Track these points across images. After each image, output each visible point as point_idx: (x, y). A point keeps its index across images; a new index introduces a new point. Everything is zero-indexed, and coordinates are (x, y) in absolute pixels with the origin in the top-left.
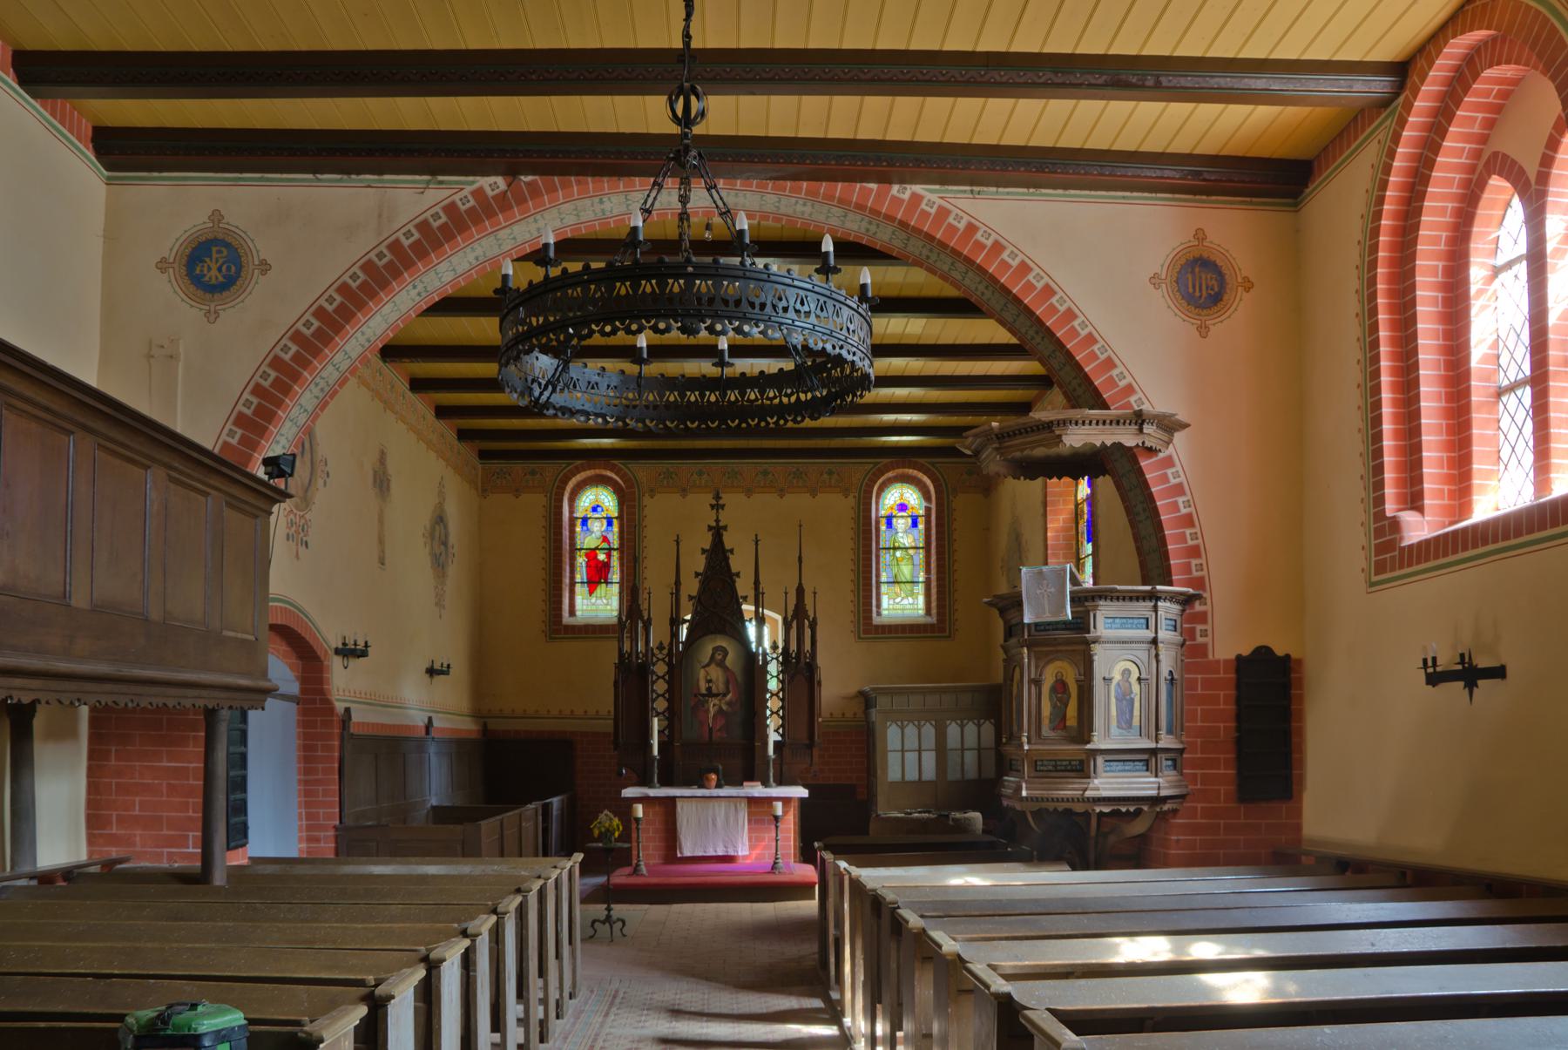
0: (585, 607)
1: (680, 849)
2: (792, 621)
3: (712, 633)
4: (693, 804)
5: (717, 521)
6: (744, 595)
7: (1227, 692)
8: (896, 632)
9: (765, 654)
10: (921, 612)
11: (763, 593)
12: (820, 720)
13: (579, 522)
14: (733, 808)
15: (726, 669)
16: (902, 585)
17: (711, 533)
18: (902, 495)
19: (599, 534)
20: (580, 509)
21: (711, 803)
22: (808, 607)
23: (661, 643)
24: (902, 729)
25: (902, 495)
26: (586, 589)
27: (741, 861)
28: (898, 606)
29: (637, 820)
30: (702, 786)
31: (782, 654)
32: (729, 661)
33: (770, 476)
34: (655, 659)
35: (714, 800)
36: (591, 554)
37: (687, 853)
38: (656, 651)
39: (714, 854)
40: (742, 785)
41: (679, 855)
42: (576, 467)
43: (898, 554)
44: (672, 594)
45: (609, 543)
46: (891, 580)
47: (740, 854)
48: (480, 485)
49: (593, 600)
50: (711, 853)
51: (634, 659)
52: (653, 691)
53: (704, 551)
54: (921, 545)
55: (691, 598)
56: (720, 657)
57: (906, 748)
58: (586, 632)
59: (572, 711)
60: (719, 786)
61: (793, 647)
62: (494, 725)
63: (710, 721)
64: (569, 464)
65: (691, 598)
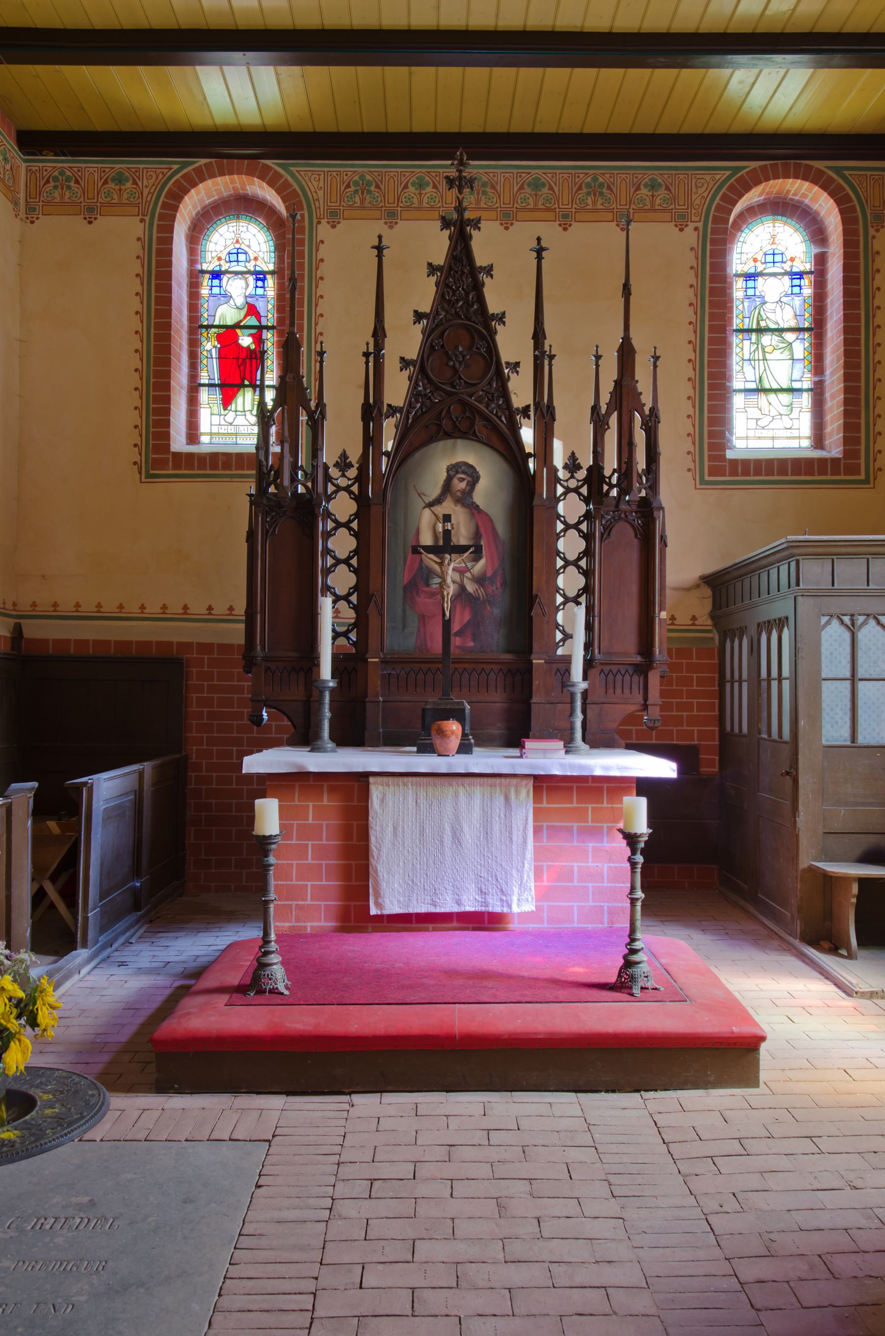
0: (215, 430)
1: (377, 895)
2: (608, 414)
3: (448, 435)
4: (409, 791)
5: (460, 209)
6: (512, 360)
7: (190, 735)
8: (770, 473)
9: (554, 480)
10: (806, 443)
11: (552, 357)
12: (664, 615)
13: (206, 280)
14: (499, 801)
15: (474, 509)
16: (772, 397)
17: (433, 279)
18: (773, 237)
19: (240, 301)
20: (209, 256)
21: (449, 790)
22: (640, 387)
23: (344, 456)
24: (853, 630)
25: (773, 237)
26: (217, 395)
27: (514, 925)
28: (765, 433)
29: (265, 842)
30: (426, 748)
31: (586, 481)
32: (480, 496)
33: (545, 190)
34: (331, 488)
35: (454, 781)
36: (228, 335)
37: (393, 906)
38: (334, 472)
39: (455, 909)
40: (521, 746)
41: (373, 911)
42: (198, 171)
43: (766, 339)
44: (366, 355)
45: (258, 317)
46: (753, 386)
47: (515, 909)
48: (22, 196)
49: (230, 416)
50: (448, 906)
51: (286, 482)
52: (327, 551)
53: (432, 269)
54: (807, 325)
55: (405, 363)
56: (463, 485)
57: (861, 673)
58: (214, 467)
59: (186, 607)
60: (464, 748)
61: (611, 463)
62: (33, 630)
63: (447, 606)
64: (184, 165)
65: (405, 363)
